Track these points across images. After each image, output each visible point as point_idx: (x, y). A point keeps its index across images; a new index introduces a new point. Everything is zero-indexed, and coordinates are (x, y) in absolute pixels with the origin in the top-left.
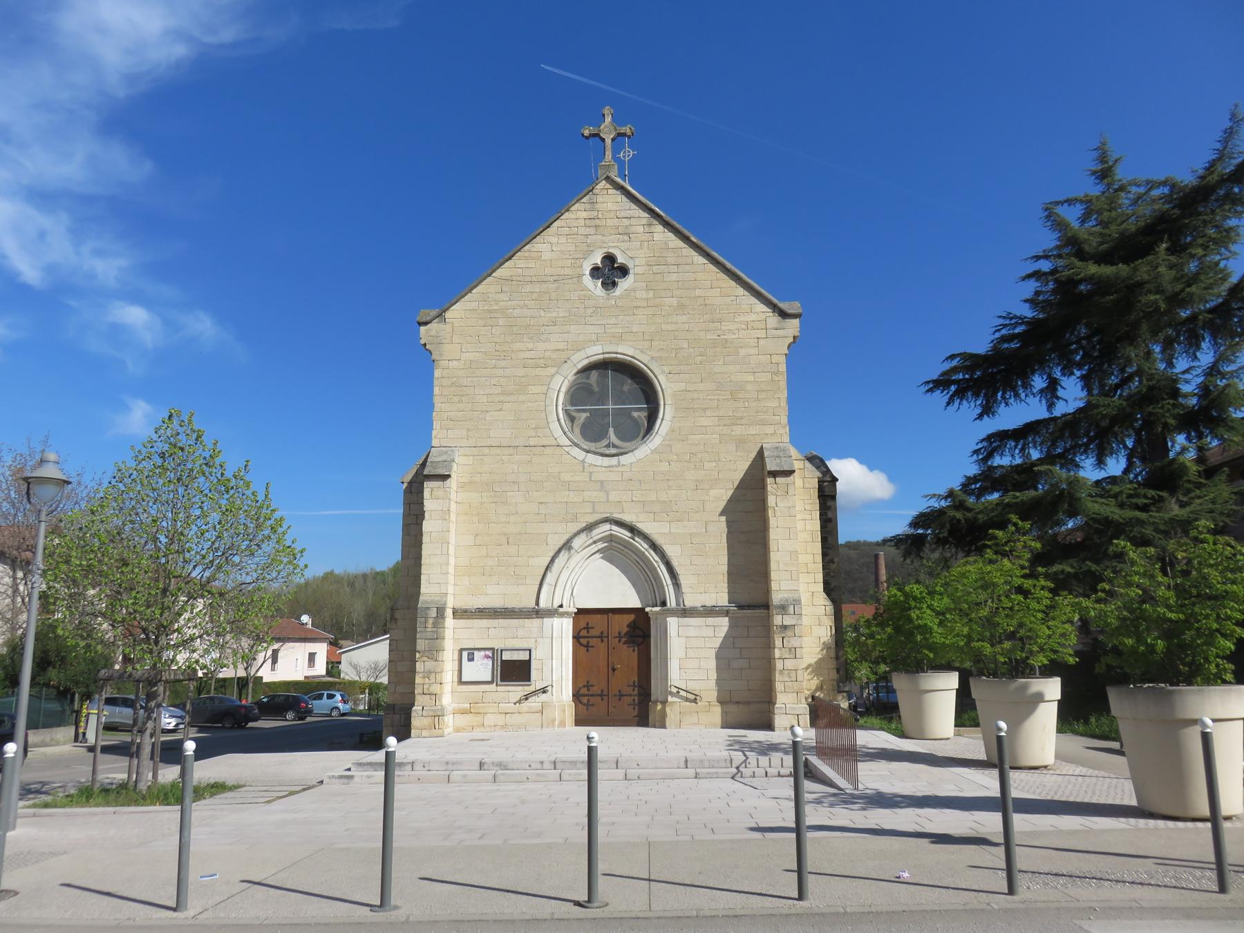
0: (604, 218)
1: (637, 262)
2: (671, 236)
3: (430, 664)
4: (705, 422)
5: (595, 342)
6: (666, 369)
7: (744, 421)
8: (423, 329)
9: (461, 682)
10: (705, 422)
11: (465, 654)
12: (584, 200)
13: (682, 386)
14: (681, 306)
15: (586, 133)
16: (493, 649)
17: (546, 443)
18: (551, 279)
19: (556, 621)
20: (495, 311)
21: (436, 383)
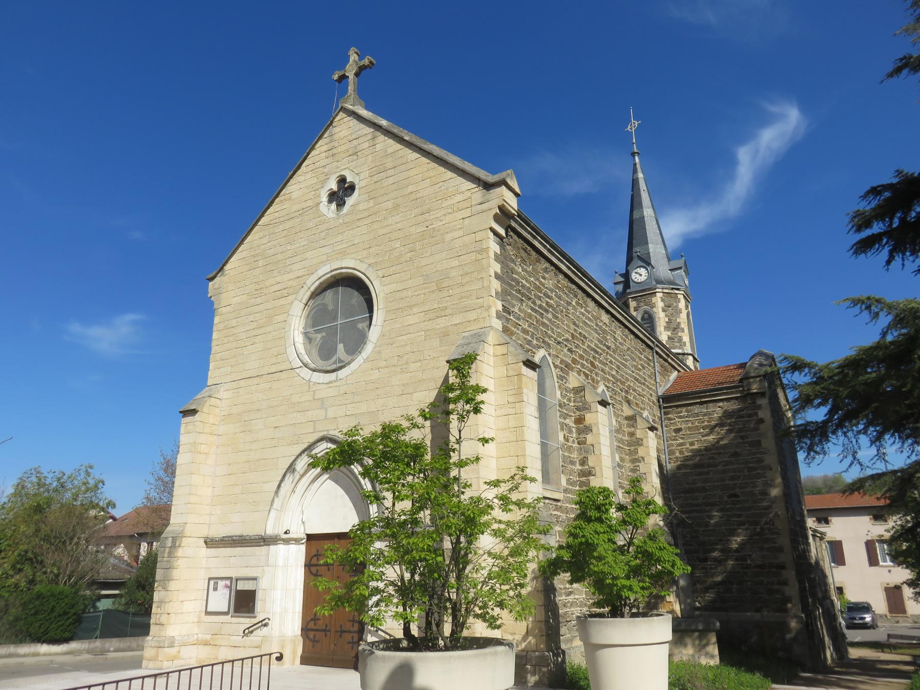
0: (350, 144)
1: (362, 176)
2: (391, 141)
3: (163, 593)
4: (411, 320)
5: (323, 263)
6: (380, 273)
7: (448, 311)
8: (211, 284)
9: (208, 613)
10: (411, 320)
11: (212, 582)
12: (326, 135)
13: (393, 287)
14: (396, 207)
15: (336, 77)
16: (231, 578)
17: (283, 368)
18: (297, 214)
19: (281, 548)
20: (257, 255)
21: (215, 328)
